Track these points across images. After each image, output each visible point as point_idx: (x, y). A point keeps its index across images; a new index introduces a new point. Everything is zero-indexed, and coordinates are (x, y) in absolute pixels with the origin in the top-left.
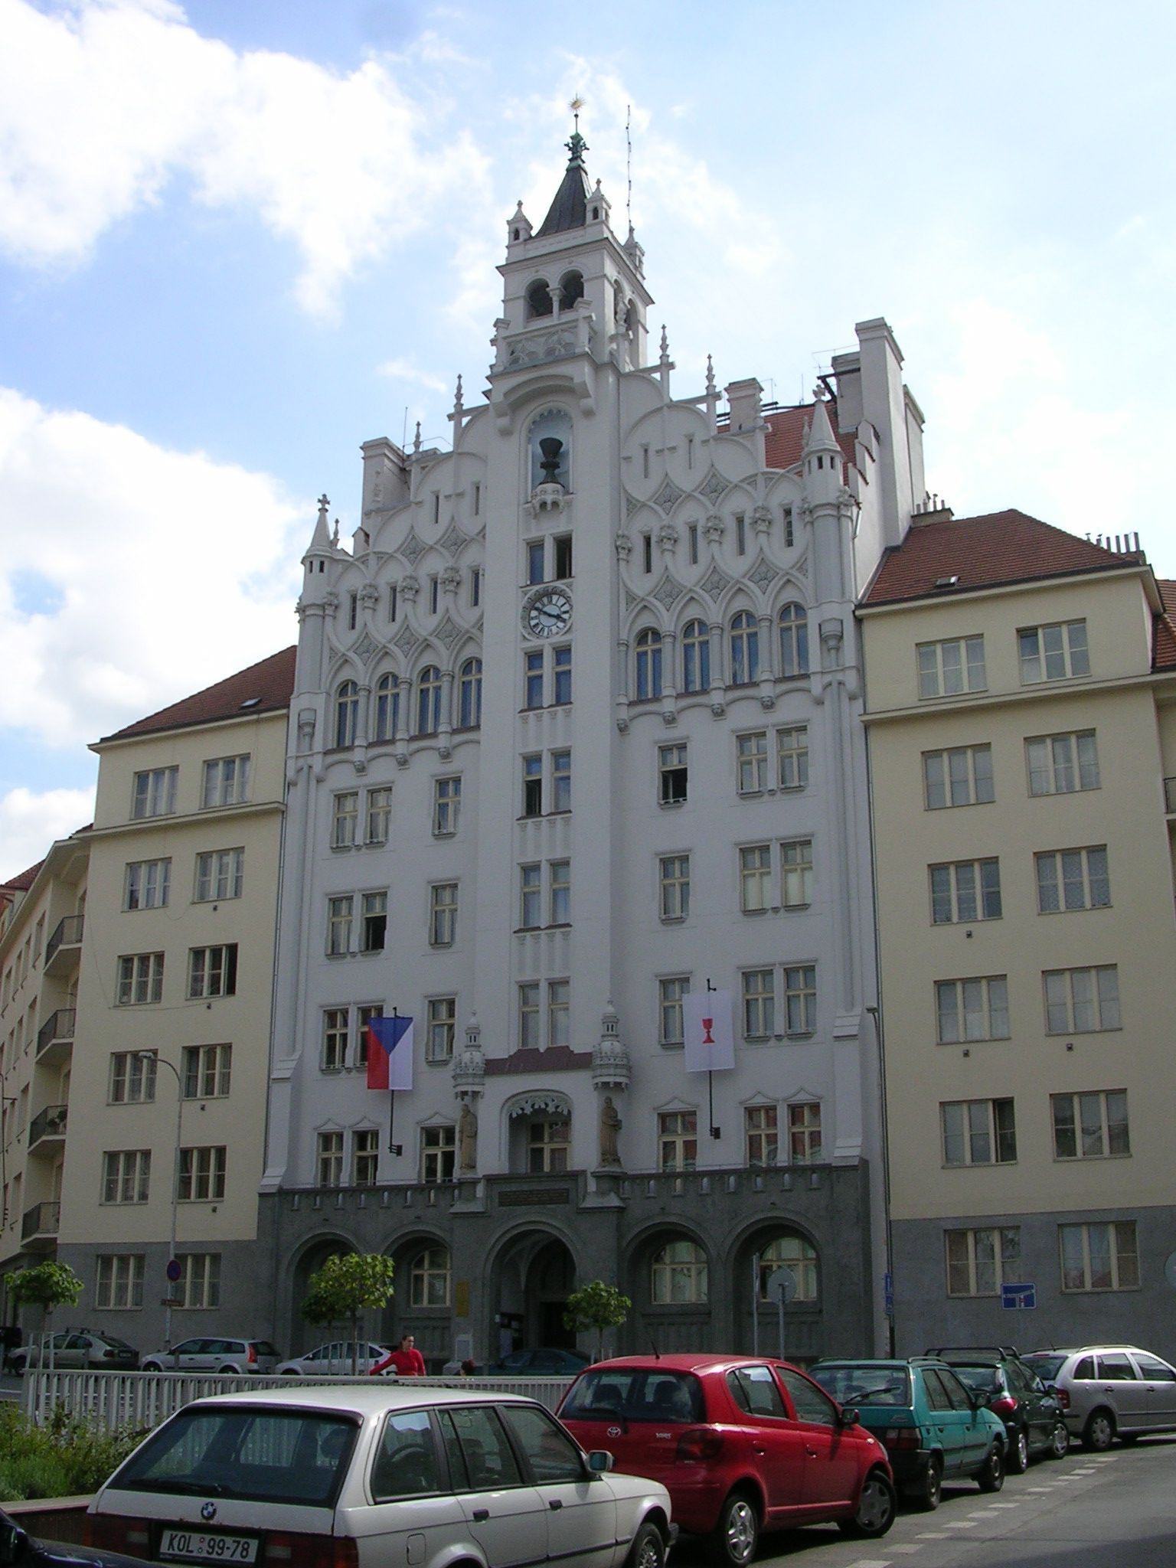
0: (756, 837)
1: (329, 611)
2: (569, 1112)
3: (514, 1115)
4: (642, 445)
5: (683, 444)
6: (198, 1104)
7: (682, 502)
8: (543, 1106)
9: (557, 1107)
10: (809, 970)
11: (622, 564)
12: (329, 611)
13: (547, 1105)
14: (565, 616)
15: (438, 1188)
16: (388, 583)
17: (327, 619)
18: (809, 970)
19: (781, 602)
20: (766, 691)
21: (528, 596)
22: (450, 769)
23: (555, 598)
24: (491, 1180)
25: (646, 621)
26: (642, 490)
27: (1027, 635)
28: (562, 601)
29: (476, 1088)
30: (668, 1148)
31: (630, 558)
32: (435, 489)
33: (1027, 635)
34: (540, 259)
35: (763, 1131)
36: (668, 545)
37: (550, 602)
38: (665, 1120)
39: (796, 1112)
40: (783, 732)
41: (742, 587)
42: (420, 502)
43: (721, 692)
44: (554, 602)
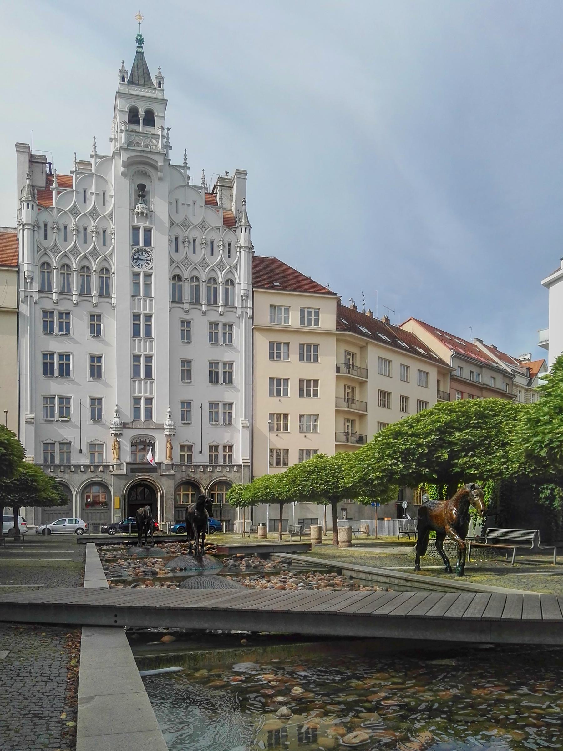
0: (66, 351)
1: (36, 229)
2: (154, 443)
3: (133, 442)
4: (83, 189)
5: (192, 204)
6: (304, 435)
7: (191, 229)
8: (144, 440)
9: (150, 441)
10: (189, 403)
11: (36, 232)
12: (36, 229)
13: (146, 440)
14: (135, 261)
15: (186, 466)
16: (228, 241)
17: (36, 231)
18: (189, 403)
19: (209, 277)
20: (187, 306)
21: (134, 249)
22: (97, 311)
23: (144, 253)
24: (128, 464)
25: (178, 272)
26: (178, 219)
27: (272, 307)
28: (147, 255)
29: (121, 432)
30: (182, 456)
31: (39, 231)
32: (177, 198)
33: (272, 307)
34: (126, 95)
35: (214, 453)
36: (186, 244)
37: (142, 254)
38: (182, 447)
39: (224, 448)
40: (61, 314)
41: (179, 266)
42: (189, 205)
43: (205, 306)
44: (144, 255)
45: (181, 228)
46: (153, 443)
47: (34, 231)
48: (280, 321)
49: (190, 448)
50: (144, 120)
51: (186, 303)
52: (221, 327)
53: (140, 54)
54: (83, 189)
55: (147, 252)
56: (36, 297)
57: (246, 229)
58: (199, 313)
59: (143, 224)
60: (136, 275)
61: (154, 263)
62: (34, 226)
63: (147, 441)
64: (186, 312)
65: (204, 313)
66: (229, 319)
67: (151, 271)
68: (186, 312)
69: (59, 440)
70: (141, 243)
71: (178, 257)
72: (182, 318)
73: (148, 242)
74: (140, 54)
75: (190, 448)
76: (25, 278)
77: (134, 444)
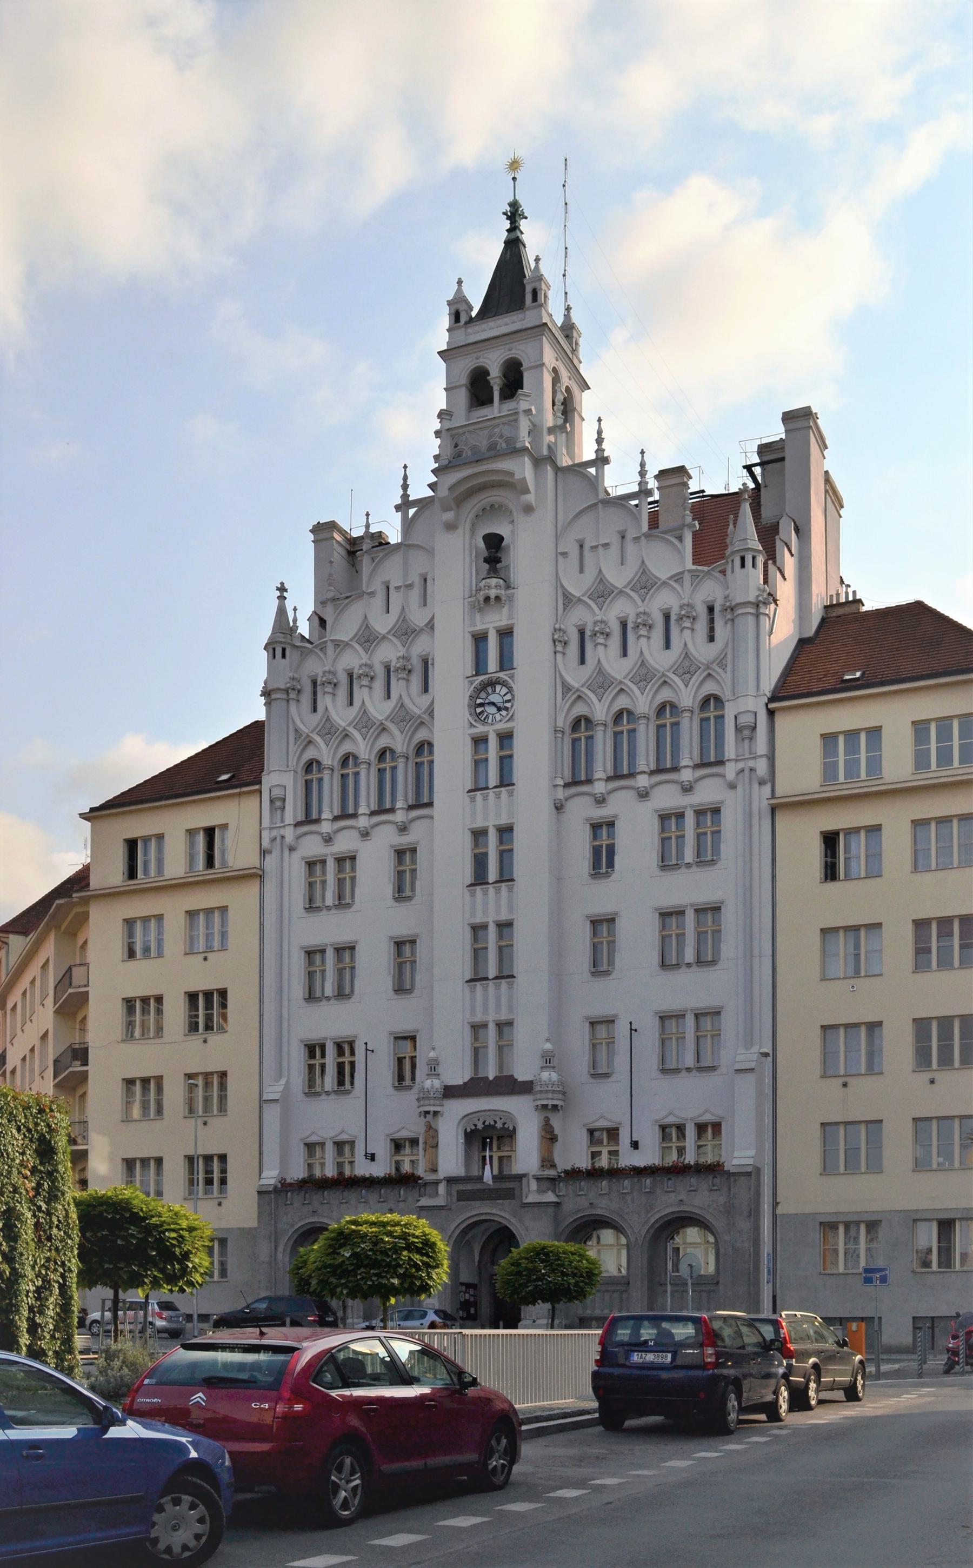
2: (514, 1128)
9: (504, 1124)
11: (559, 656)
12: (293, 695)
13: (495, 1122)
20: (686, 775)
21: (508, 679)
23: (498, 688)
24: (450, 1181)
26: (578, 586)
28: (504, 690)
31: (695, 627)
37: (494, 691)
40: (340, 861)
45: (590, 606)
46: (511, 1128)
47: (288, 701)
48: (852, 768)
49: (613, 1133)
50: (502, 390)
51: (362, 815)
52: (690, 819)
53: (513, 245)
54: (577, 541)
55: (504, 684)
56: (289, 833)
57: (754, 558)
58: (631, 794)
59: (492, 622)
60: (479, 741)
61: (520, 707)
62: (758, 606)
63: (480, 1126)
64: (687, 789)
65: (644, 795)
66: (346, 842)
67: (509, 725)
68: (601, 801)
69: (333, 1134)
70: (492, 663)
71: (576, 677)
72: (592, 819)
73: (506, 662)
74: (513, 245)
75: (613, 1133)
76: (272, 801)
77: (470, 1136)
